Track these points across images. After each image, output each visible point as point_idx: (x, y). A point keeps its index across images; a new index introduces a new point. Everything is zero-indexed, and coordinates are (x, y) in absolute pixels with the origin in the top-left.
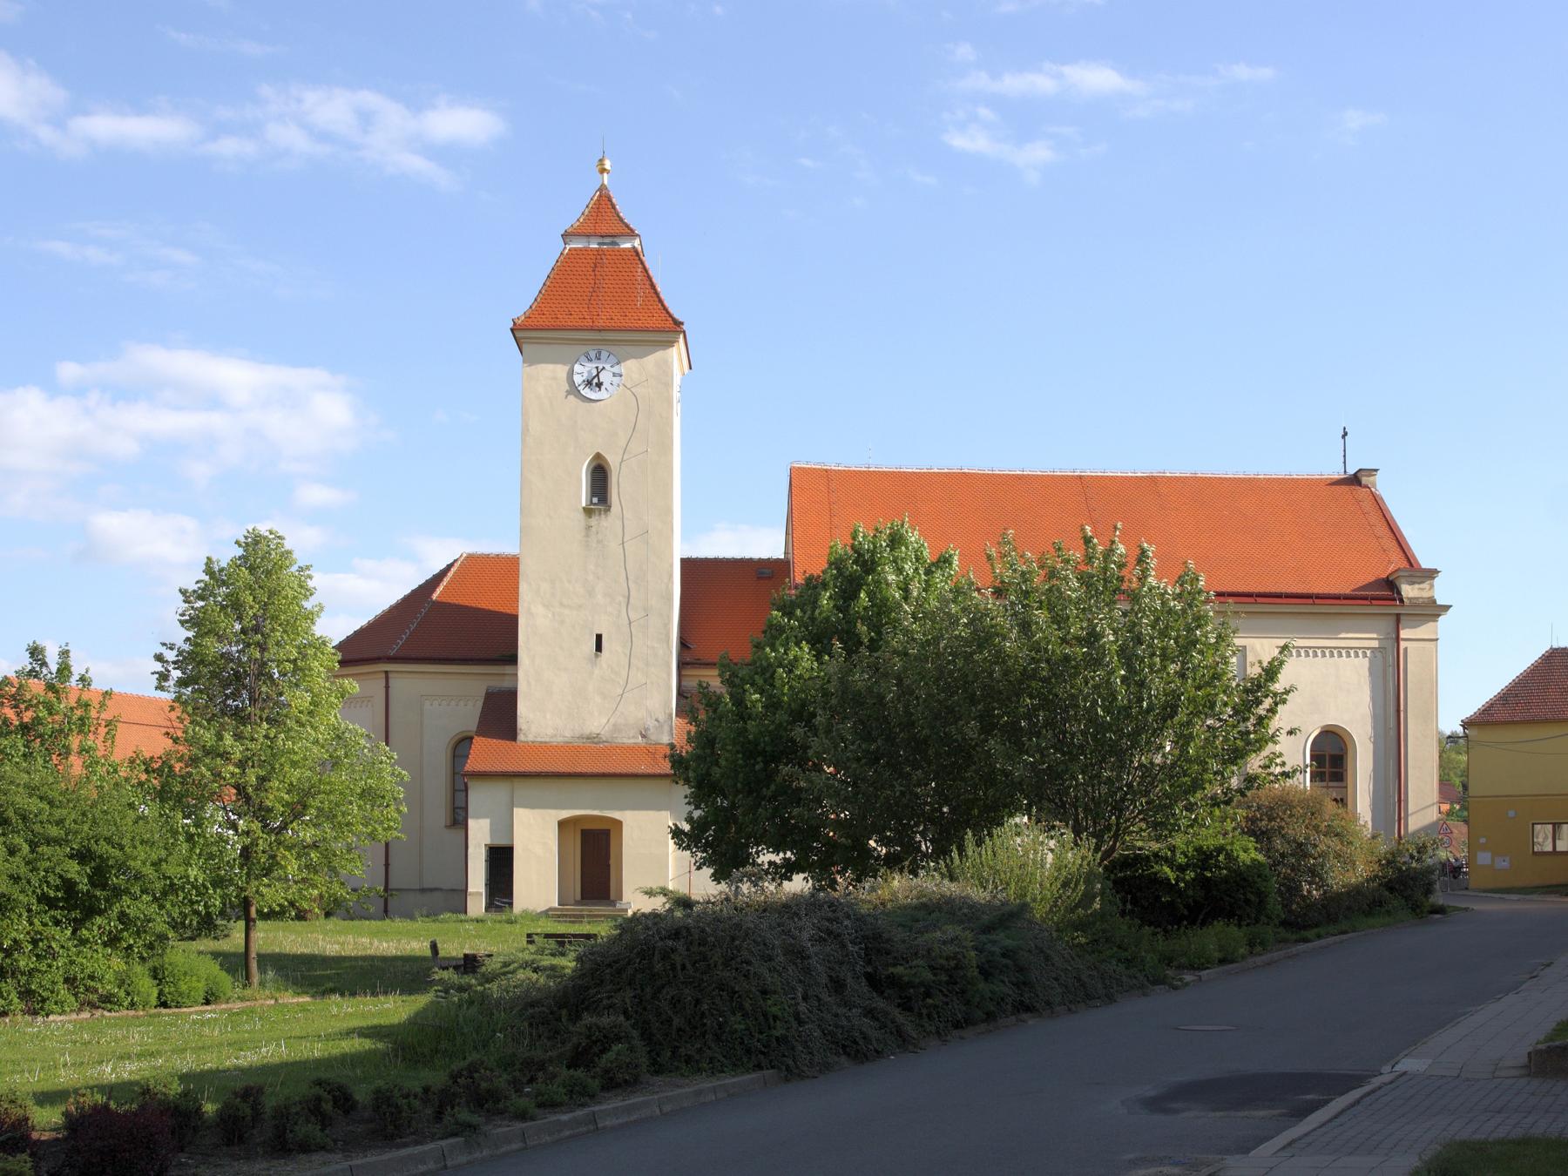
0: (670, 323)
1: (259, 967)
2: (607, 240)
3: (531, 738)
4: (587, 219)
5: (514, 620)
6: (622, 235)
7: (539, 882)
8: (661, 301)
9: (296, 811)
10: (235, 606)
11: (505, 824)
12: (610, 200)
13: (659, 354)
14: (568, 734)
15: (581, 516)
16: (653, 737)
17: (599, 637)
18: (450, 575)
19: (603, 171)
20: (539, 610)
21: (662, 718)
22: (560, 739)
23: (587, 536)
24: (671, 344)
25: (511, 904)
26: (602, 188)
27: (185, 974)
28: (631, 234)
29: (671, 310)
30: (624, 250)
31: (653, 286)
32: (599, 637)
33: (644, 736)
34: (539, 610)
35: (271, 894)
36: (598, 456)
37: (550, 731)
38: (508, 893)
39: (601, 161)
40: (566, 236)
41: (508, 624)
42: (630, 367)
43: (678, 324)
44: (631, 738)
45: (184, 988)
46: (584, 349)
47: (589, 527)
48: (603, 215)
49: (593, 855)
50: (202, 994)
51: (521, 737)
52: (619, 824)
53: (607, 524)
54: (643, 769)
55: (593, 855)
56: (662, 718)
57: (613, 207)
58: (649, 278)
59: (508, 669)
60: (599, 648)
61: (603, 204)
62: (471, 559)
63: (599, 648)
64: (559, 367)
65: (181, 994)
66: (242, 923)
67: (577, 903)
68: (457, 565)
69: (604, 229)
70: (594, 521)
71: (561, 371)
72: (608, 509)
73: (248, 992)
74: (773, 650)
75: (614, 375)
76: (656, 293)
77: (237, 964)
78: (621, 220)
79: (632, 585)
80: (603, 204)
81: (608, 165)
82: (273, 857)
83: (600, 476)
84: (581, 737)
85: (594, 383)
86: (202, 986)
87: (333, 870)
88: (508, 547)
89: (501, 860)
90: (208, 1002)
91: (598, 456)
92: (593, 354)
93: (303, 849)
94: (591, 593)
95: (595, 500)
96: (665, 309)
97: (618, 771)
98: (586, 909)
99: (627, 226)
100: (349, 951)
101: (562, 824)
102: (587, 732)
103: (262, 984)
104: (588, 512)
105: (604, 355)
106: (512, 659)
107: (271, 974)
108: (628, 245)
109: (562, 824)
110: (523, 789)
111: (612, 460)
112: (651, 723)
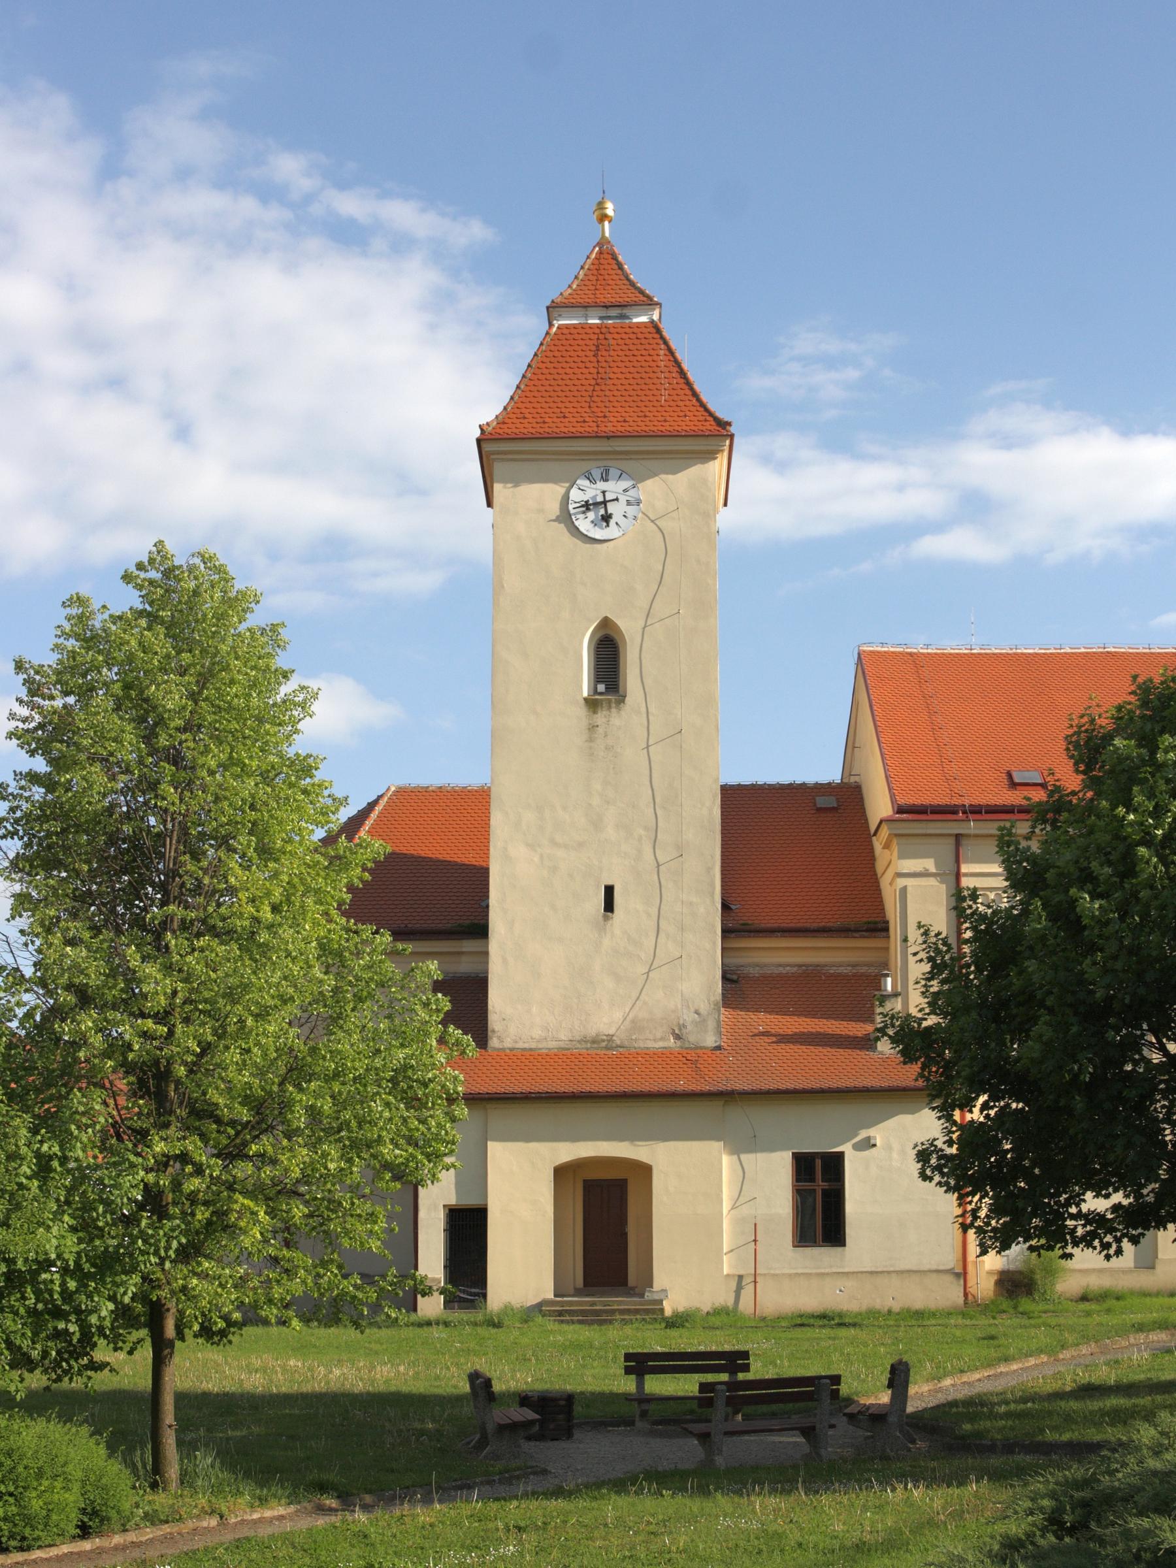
0: (710, 425)
1: (180, 1443)
2: (614, 312)
3: (508, 1044)
4: (583, 284)
5: (480, 877)
6: (636, 304)
7: (525, 1260)
8: (695, 394)
9: (267, 1113)
10: (136, 701)
11: (476, 1174)
12: (615, 258)
13: (695, 471)
14: (564, 1036)
15: (582, 711)
16: (692, 1038)
17: (609, 891)
18: (374, 815)
19: (603, 218)
20: (519, 851)
21: (704, 1008)
22: (552, 1044)
23: (591, 740)
24: (710, 455)
25: (485, 1296)
26: (603, 243)
27: (40, 1474)
28: (649, 302)
29: (711, 407)
30: (639, 325)
31: (682, 374)
32: (609, 891)
33: (678, 1037)
34: (519, 851)
35: (211, 1286)
36: (606, 623)
37: (537, 1033)
38: (480, 1280)
39: (601, 206)
40: (553, 309)
41: (475, 880)
42: (653, 489)
43: (724, 424)
44: (658, 1040)
45: (36, 1505)
46: (585, 466)
47: (593, 728)
48: (606, 282)
49: (605, 1222)
50: (75, 1516)
51: (494, 1043)
52: (644, 1171)
53: (625, 721)
54: (681, 1085)
55: (605, 1222)
56: (704, 1008)
57: (620, 266)
58: (677, 363)
59: (469, 945)
60: (609, 906)
61: (605, 262)
62: (404, 796)
63: (609, 906)
64: (550, 487)
65: (29, 1520)
66: (146, 1353)
67: (578, 1292)
68: (383, 802)
69: (609, 299)
70: (600, 718)
71: (559, 490)
72: (622, 700)
73: (161, 1500)
74: (1130, 808)
75: (629, 503)
76: (689, 384)
77: (132, 1425)
78: (632, 284)
79: (659, 812)
80: (605, 262)
81: (610, 210)
82: (221, 1214)
83: (608, 653)
84: (584, 1040)
85: (602, 511)
86: (72, 1498)
87: (330, 1240)
88: (463, 773)
89: (468, 1229)
90: (84, 1532)
91: (606, 623)
92: (596, 473)
93: (274, 1194)
94: (597, 824)
95: (601, 688)
96: (703, 405)
97: (646, 1087)
98: (599, 1302)
99: (642, 292)
100: (282, 1385)
101: (561, 1172)
102: (592, 1032)
103: (186, 1479)
104: (592, 704)
105: (614, 472)
106: (480, 931)
107: (205, 1460)
108: (644, 319)
109: (561, 1172)
110: (498, 1116)
111: (628, 627)
112: (689, 1017)
